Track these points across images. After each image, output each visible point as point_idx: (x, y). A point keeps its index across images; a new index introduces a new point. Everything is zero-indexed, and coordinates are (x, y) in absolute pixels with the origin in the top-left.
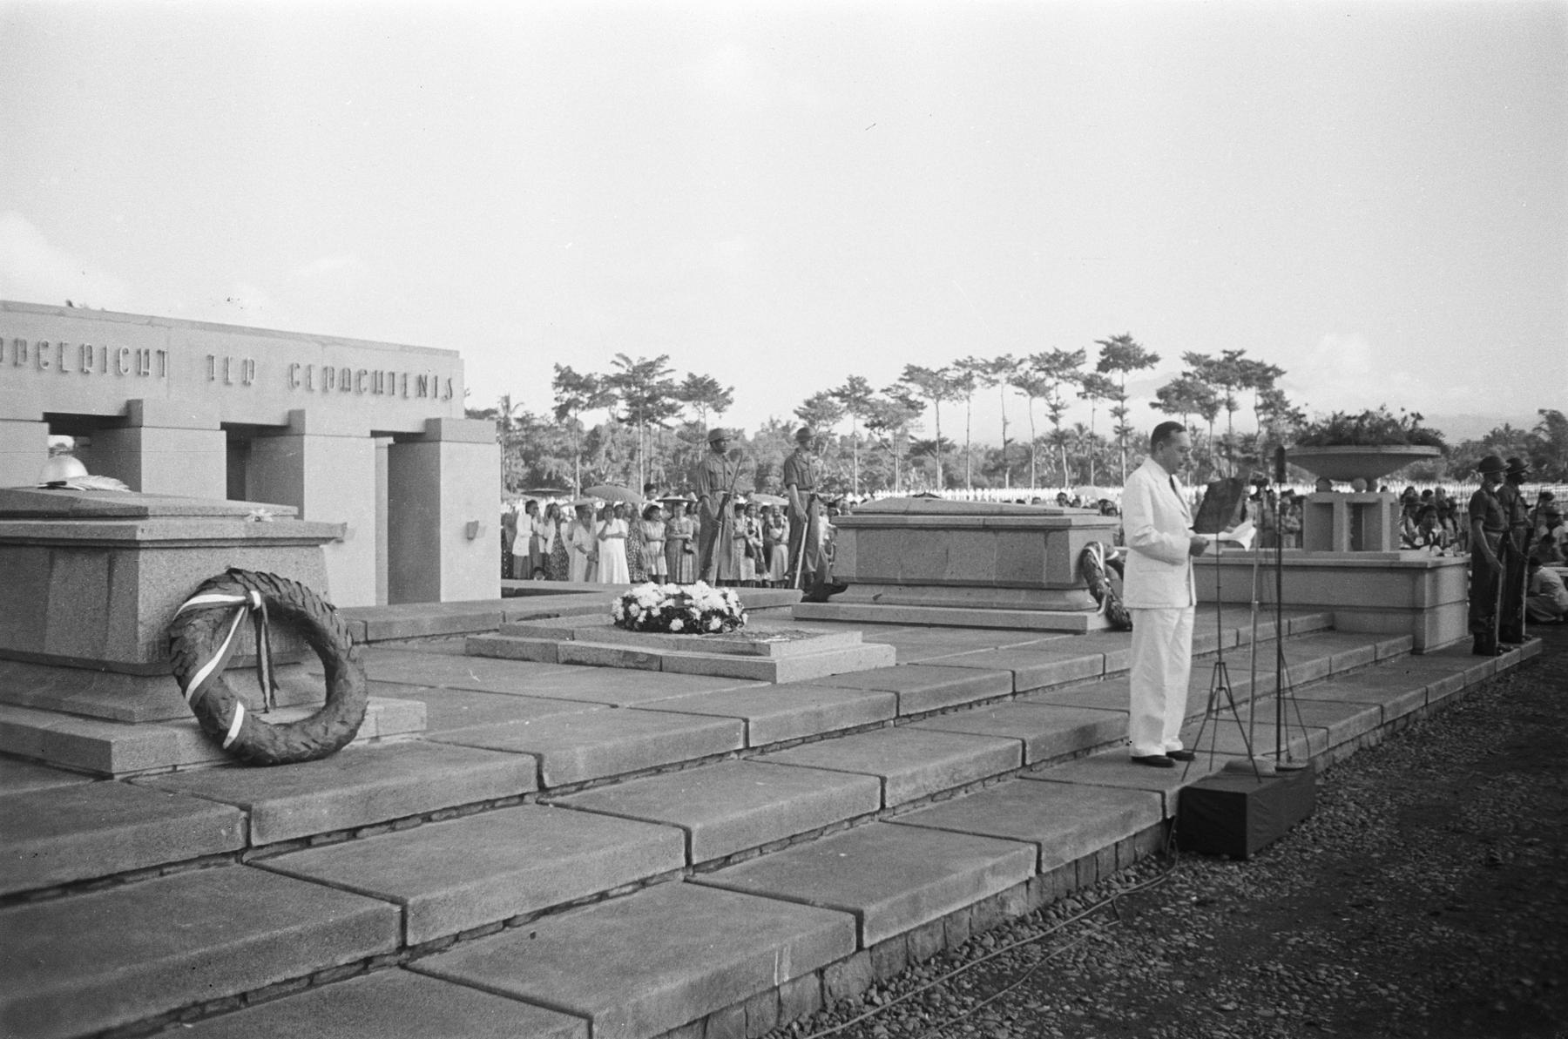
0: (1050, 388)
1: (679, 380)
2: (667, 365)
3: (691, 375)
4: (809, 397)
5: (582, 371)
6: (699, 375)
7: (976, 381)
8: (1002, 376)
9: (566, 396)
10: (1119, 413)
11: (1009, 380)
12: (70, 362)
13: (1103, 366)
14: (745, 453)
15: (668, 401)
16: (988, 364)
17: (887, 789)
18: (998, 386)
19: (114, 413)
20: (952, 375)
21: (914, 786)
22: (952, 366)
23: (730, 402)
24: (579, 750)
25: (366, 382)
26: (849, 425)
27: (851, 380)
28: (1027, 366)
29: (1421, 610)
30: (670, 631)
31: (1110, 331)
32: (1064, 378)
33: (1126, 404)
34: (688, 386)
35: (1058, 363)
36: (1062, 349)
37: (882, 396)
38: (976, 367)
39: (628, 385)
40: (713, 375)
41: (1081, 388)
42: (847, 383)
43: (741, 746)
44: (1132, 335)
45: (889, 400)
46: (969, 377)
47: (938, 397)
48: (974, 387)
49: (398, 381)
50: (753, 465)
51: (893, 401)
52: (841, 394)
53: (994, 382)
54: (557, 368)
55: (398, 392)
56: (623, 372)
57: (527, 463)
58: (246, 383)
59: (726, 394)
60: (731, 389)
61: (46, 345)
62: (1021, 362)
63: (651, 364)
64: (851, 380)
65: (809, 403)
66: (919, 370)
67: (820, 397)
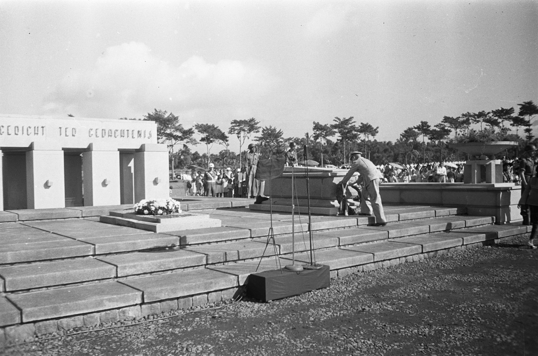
0: (499, 123)
1: (358, 125)
2: (353, 121)
3: (362, 123)
4: (406, 129)
5: (323, 124)
6: (365, 123)
7: (471, 121)
8: (481, 119)
9: (318, 132)
10: (528, 131)
11: (484, 121)
12: (12, 131)
13: (521, 114)
14: (390, 150)
15: (354, 132)
16: (475, 115)
17: (118, 270)
18: (480, 123)
19: (28, 146)
20: (461, 119)
21: (135, 270)
22: (461, 116)
23: (377, 132)
24: (8, 253)
25: (118, 133)
26: (423, 139)
27: (422, 122)
28: (491, 115)
29: (499, 207)
30: (144, 214)
31: (524, 100)
32: (505, 119)
33: (531, 127)
34: (361, 127)
35: (504, 113)
36: (504, 108)
37: (435, 128)
38: (471, 116)
39: (340, 128)
40: (370, 123)
41: (512, 122)
42: (420, 124)
43: (92, 253)
44: (533, 102)
45: (438, 129)
46: (468, 120)
47: (456, 128)
48: (470, 123)
49: (130, 132)
50: (392, 154)
51: (439, 130)
52: (418, 128)
53: (478, 122)
54: (314, 123)
55: (130, 136)
56: (338, 123)
57: (313, 156)
58: (73, 135)
59: (375, 130)
60: (378, 128)
61: (117, 131)
62: (489, 113)
63: (347, 120)
64: (422, 122)
65: (405, 131)
66: (449, 118)
67: (410, 129)
